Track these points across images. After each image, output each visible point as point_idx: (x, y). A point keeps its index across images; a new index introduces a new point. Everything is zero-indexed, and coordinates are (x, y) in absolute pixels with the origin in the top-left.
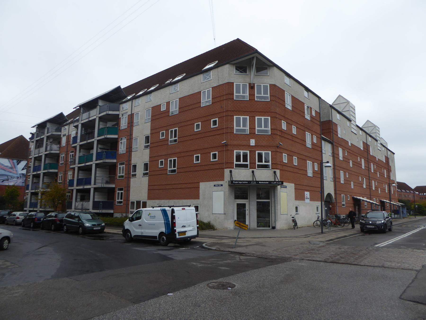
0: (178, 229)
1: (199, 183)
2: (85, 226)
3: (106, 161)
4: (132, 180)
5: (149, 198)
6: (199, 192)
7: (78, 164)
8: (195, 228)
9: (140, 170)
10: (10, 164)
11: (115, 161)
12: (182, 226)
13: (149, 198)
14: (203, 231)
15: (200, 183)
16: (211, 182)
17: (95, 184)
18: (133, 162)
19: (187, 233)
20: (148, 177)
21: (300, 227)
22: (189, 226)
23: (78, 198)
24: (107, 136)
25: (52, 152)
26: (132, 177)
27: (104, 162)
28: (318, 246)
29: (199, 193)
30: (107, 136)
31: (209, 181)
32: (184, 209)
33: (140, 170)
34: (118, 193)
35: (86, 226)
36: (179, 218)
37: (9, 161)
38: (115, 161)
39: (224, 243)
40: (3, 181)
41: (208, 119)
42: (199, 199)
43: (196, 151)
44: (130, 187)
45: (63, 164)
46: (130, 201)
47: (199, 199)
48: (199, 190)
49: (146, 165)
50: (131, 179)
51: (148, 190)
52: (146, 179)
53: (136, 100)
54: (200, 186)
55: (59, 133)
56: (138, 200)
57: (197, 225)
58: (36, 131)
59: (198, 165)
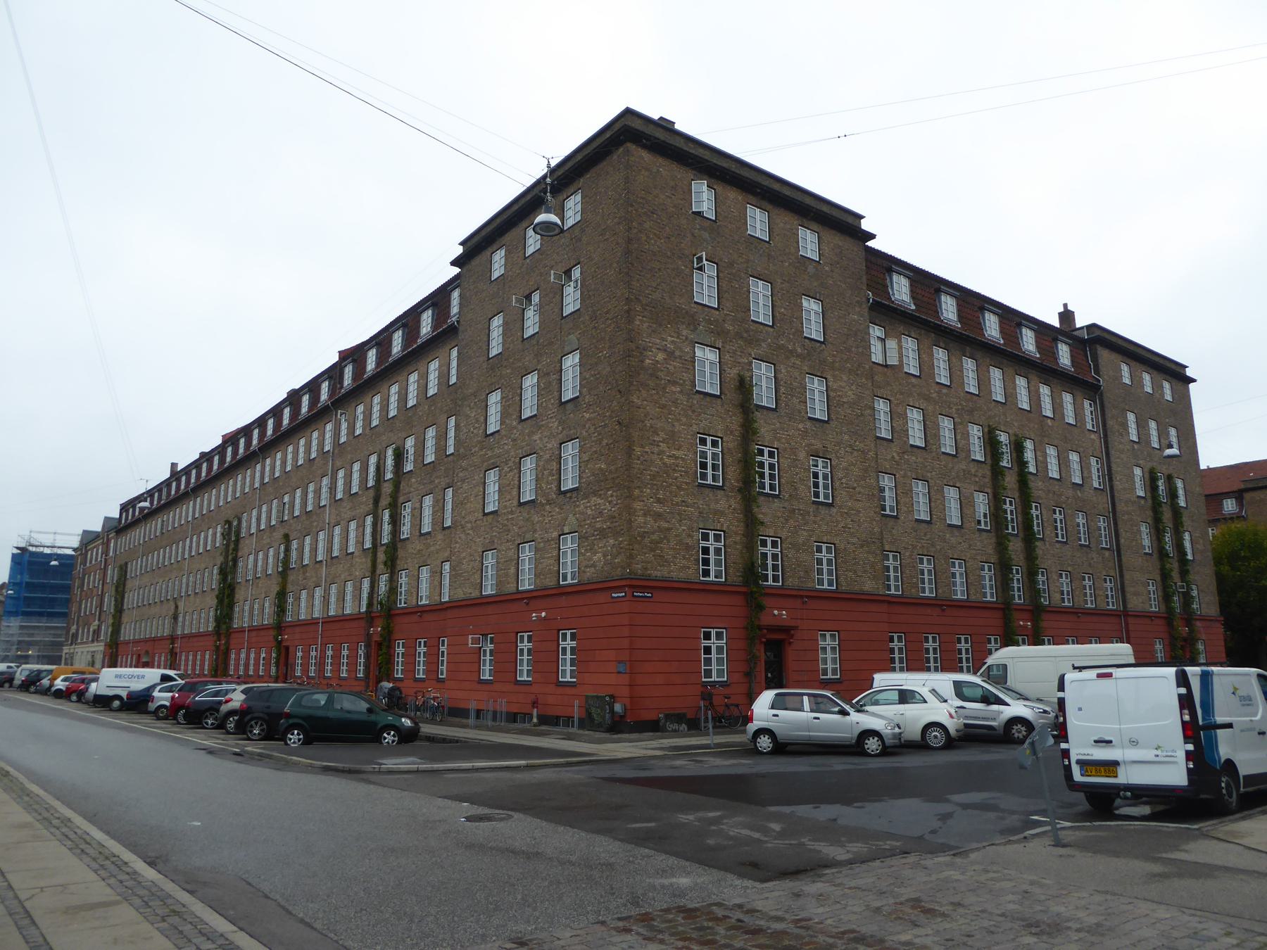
8: (1173, 754)
12: (1095, 742)
19: (1121, 771)
22: (1134, 743)
32: (1109, 675)
36: (1080, 709)
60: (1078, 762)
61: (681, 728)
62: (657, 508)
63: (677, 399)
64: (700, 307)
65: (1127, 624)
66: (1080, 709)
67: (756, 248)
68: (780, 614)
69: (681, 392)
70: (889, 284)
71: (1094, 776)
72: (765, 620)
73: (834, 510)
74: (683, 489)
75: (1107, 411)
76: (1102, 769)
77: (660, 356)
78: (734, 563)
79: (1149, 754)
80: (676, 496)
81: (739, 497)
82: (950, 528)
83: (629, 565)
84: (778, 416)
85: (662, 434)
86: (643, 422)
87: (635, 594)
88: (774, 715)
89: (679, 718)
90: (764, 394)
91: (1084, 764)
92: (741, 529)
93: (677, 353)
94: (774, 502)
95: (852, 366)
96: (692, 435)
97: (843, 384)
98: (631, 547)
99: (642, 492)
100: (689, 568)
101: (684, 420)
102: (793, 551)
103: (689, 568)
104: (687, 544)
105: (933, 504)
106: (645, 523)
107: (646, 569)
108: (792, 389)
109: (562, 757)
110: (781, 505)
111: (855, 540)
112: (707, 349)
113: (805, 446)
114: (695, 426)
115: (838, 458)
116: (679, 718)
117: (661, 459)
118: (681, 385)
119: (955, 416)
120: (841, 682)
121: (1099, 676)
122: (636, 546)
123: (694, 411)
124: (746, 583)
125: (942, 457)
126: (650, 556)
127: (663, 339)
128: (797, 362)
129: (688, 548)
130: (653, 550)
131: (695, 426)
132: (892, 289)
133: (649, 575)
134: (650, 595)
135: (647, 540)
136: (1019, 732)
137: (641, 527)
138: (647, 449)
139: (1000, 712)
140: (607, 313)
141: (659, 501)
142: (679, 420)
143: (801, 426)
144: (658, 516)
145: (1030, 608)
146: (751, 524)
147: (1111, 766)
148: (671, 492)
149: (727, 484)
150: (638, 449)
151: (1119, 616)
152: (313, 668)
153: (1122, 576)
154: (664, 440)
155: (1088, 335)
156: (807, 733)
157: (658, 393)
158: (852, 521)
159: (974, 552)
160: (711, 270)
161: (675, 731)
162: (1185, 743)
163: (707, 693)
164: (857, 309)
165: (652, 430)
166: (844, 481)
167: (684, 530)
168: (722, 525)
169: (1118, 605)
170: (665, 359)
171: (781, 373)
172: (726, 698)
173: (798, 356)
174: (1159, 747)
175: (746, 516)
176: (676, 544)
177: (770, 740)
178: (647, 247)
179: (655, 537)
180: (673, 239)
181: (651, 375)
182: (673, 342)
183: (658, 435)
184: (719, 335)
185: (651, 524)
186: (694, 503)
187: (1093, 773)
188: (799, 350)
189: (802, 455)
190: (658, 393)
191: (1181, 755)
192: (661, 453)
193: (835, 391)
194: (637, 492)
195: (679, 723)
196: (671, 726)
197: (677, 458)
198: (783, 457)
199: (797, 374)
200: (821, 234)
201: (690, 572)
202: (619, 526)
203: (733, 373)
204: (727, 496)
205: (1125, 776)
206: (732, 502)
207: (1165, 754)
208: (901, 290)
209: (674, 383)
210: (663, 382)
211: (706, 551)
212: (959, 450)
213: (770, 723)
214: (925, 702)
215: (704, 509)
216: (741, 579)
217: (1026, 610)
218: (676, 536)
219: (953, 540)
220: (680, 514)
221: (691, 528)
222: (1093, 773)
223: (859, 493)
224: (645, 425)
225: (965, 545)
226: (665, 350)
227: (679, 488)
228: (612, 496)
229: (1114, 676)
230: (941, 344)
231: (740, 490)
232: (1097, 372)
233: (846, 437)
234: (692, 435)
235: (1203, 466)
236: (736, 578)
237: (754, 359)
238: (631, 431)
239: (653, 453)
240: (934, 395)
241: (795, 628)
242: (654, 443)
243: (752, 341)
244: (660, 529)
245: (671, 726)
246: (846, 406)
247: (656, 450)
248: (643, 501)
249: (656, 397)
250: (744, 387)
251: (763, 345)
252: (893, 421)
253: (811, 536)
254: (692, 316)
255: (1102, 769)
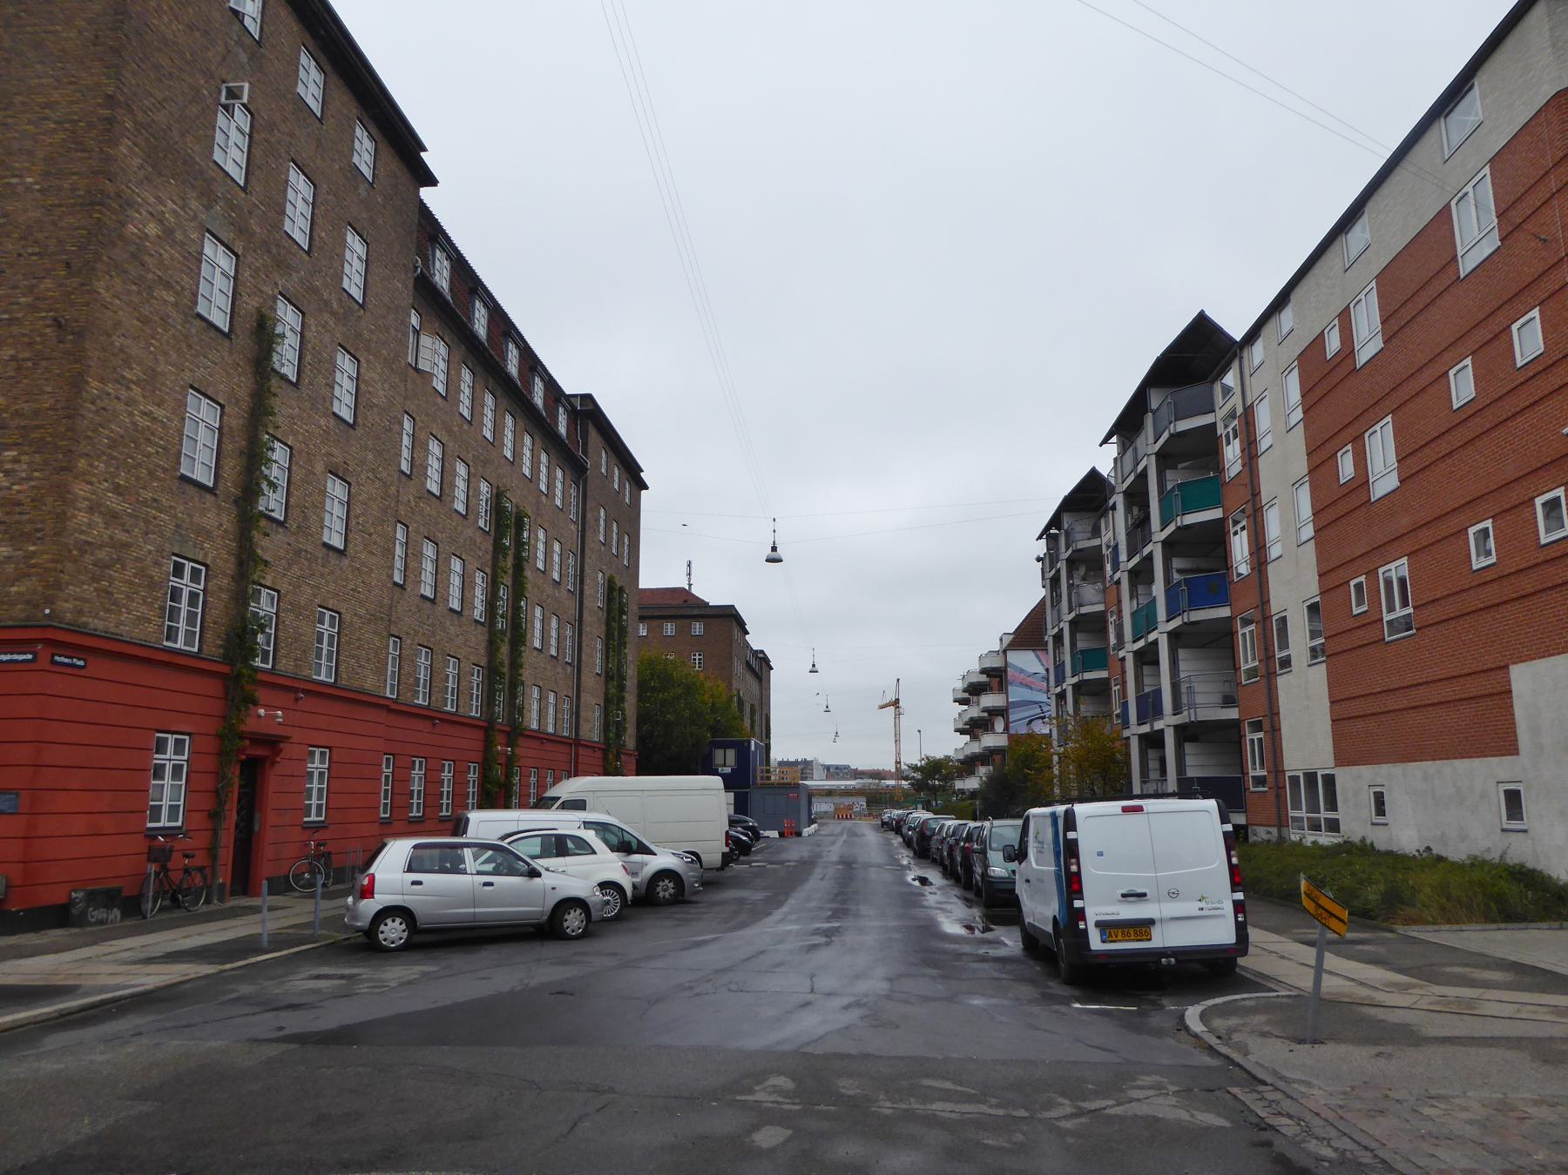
0: (1098, 906)
1: (1506, 667)
2: (992, 874)
3: (1192, 619)
4: (1281, 681)
5: (1342, 759)
6: (1513, 715)
7: (1134, 642)
8: (1219, 906)
9: (1300, 641)
10: (1043, 665)
11: (1225, 612)
12: (1124, 896)
13: (1342, 759)
14: (1503, 926)
15: (1511, 667)
16: (1558, 657)
17: (1177, 710)
18: (1275, 607)
19: (1156, 932)
20: (1324, 666)
21: (257, 923)
22: (1174, 895)
23: (1150, 766)
24: (1182, 522)
25: (1084, 610)
26: (1281, 668)
27: (1185, 623)
28: (295, 1023)
29: (1514, 724)
30: (1182, 522)
31: (1549, 656)
32: (1139, 809)
33: (1300, 641)
34: (1252, 741)
35: (992, 877)
36: (1100, 854)
37: (1037, 656)
38: (1225, 612)
39: (1372, 1011)
40: (1030, 722)
41: (1497, 331)
42: (1518, 754)
43: (1471, 507)
44: (1278, 713)
45: (1411, 629)
46: (1288, 774)
47: (1518, 754)
48: (1512, 706)
49: (1313, 609)
50: (1279, 679)
51: (1330, 722)
52: (1321, 672)
53: (1254, 347)
54: (1514, 687)
55: (1096, 542)
56: (1309, 766)
57: (1233, 891)
58: (1048, 549)
59: (1489, 579)
60: (1098, 924)
61: (111, 917)
62: (113, 502)
63: (169, 317)
64: (222, 174)
65: (577, 755)
66: (1100, 854)
67: (305, 119)
68: (268, 715)
69: (175, 305)
70: (431, 257)
71: (1120, 941)
72: (250, 725)
73: (346, 562)
74: (159, 479)
75: (588, 501)
76: (1132, 931)
77: (152, 229)
78: (215, 623)
79: (1191, 908)
80: (144, 488)
81: (234, 510)
82: (452, 614)
83: (50, 601)
84: (298, 397)
85: (137, 370)
86: (109, 336)
87: (57, 658)
88: (414, 883)
89: (108, 898)
90: (286, 359)
91: (1105, 927)
92: (230, 567)
93: (179, 236)
94: (277, 533)
95: (389, 355)
96: (182, 387)
97: (377, 377)
98: (59, 566)
99: (91, 465)
100: (149, 621)
101: (174, 356)
102: (292, 616)
103: (149, 621)
104: (152, 577)
105: (439, 576)
106: (89, 525)
107: (80, 612)
108: (320, 361)
109: (29, 1006)
110: (286, 540)
111: (362, 612)
112: (221, 248)
113: (325, 455)
114: (188, 373)
115: (359, 484)
116: (108, 898)
117: (131, 414)
118: (177, 293)
119: (471, 464)
120: (326, 827)
121: (1125, 810)
122: (69, 566)
123: (190, 347)
124: (228, 658)
125: (454, 515)
126: (89, 590)
127: (161, 202)
128: (331, 323)
129: (153, 585)
130: (95, 579)
131: (188, 373)
132: (434, 266)
133: (85, 625)
134: (81, 663)
135: (88, 558)
136: (665, 890)
137: (82, 532)
138: (110, 388)
139: (644, 864)
140: (48, 106)
141: (117, 489)
142: (166, 354)
143: (322, 422)
144: (112, 517)
145: (508, 729)
146: (247, 562)
147: (1143, 927)
148: (138, 478)
149: (221, 487)
150: (95, 384)
151: (571, 744)
152: (416, 788)
153: (578, 697)
154: (138, 380)
155: (581, 405)
156: (472, 910)
157: (139, 293)
158: (363, 582)
159: (468, 649)
160: (242, 119)
161: (101, 922)
162: (1233, 891)
163: (158, 850)
164: (403, 276)
165: (122, 355)
166: (361, 520)
167: (150, 552)
168: (206, 555)
169: (571, 732)
170: (158, 236)
171: (311, 331)
172: (186, 856)
173: (334, 314)
174: (1204, 898)
175: (240, 547)
176: (135, 575)
177: (403, 926)
178: (155, 22)
179: (102, 555)
180: (197, 34)
181: (134, 256)
182: (174, 212)
183: (131, 369)
184: (241, 232)
185: (100, 531)
186: (171, 507)
187: (1120, 937)
188: (335, 305)
189: (319, 467)
190: (139, 293)
191: (1229, 908)
192: (130, 402)
193: (365, 382)
194: (82, 464)
195: (108, 907)
196: (97, 914)
197: (154, 419)
198: (297, 463)
199: (327, 339)
200: (380, 145)
201: (151, 628)
202: (31, 521)
203: (250, 303)
204: (219, 507)
205: (1161, 939)
206: (225, 518)
207: (1210, 906)
208: (442, 276)
209: (168, 286)
210: (150, 276)
211: (176, 594)
212: (470, 511)
213: (406, 897)
214: (594, 852)
215: (183, 521)
216: (221, 651)
217: (475, 726)
218: (137, 559)
219: (453, 630)
220: (146, 521)
221: (160, 550)
222: (1120, 937)
223: (375, 543)
224: (112, 344)
225: (461, 640)
226: (161, 222)
227: (151, 473)
228: (16, 461)
229: (1145, 811)
230: (470, 365)
231: (236, 502)
232: (585, 452)
233: (370, 456)
234: (182, 387)
235: (642, 585)
236: (214, 649)
237: (281, 294)
238: (87, 345)
239: (118, 398)
240: (456, 429)
241: (286, 739)
242: (121, 381)
243: (282, 265)
244: (114, 544)
245: (94, 913)
246: (375, 410)
247: (124, 394)
248: (91, 483)
249: (136, 299)
250: (264, 334)
251: (294, 275)
252: (415, 451)
253: (315, 596)
254: (208, 181)
255: (1132, 931)
